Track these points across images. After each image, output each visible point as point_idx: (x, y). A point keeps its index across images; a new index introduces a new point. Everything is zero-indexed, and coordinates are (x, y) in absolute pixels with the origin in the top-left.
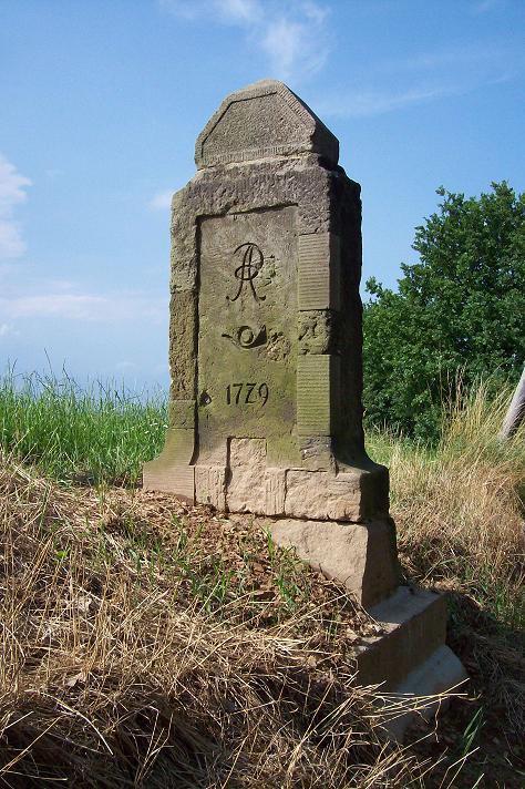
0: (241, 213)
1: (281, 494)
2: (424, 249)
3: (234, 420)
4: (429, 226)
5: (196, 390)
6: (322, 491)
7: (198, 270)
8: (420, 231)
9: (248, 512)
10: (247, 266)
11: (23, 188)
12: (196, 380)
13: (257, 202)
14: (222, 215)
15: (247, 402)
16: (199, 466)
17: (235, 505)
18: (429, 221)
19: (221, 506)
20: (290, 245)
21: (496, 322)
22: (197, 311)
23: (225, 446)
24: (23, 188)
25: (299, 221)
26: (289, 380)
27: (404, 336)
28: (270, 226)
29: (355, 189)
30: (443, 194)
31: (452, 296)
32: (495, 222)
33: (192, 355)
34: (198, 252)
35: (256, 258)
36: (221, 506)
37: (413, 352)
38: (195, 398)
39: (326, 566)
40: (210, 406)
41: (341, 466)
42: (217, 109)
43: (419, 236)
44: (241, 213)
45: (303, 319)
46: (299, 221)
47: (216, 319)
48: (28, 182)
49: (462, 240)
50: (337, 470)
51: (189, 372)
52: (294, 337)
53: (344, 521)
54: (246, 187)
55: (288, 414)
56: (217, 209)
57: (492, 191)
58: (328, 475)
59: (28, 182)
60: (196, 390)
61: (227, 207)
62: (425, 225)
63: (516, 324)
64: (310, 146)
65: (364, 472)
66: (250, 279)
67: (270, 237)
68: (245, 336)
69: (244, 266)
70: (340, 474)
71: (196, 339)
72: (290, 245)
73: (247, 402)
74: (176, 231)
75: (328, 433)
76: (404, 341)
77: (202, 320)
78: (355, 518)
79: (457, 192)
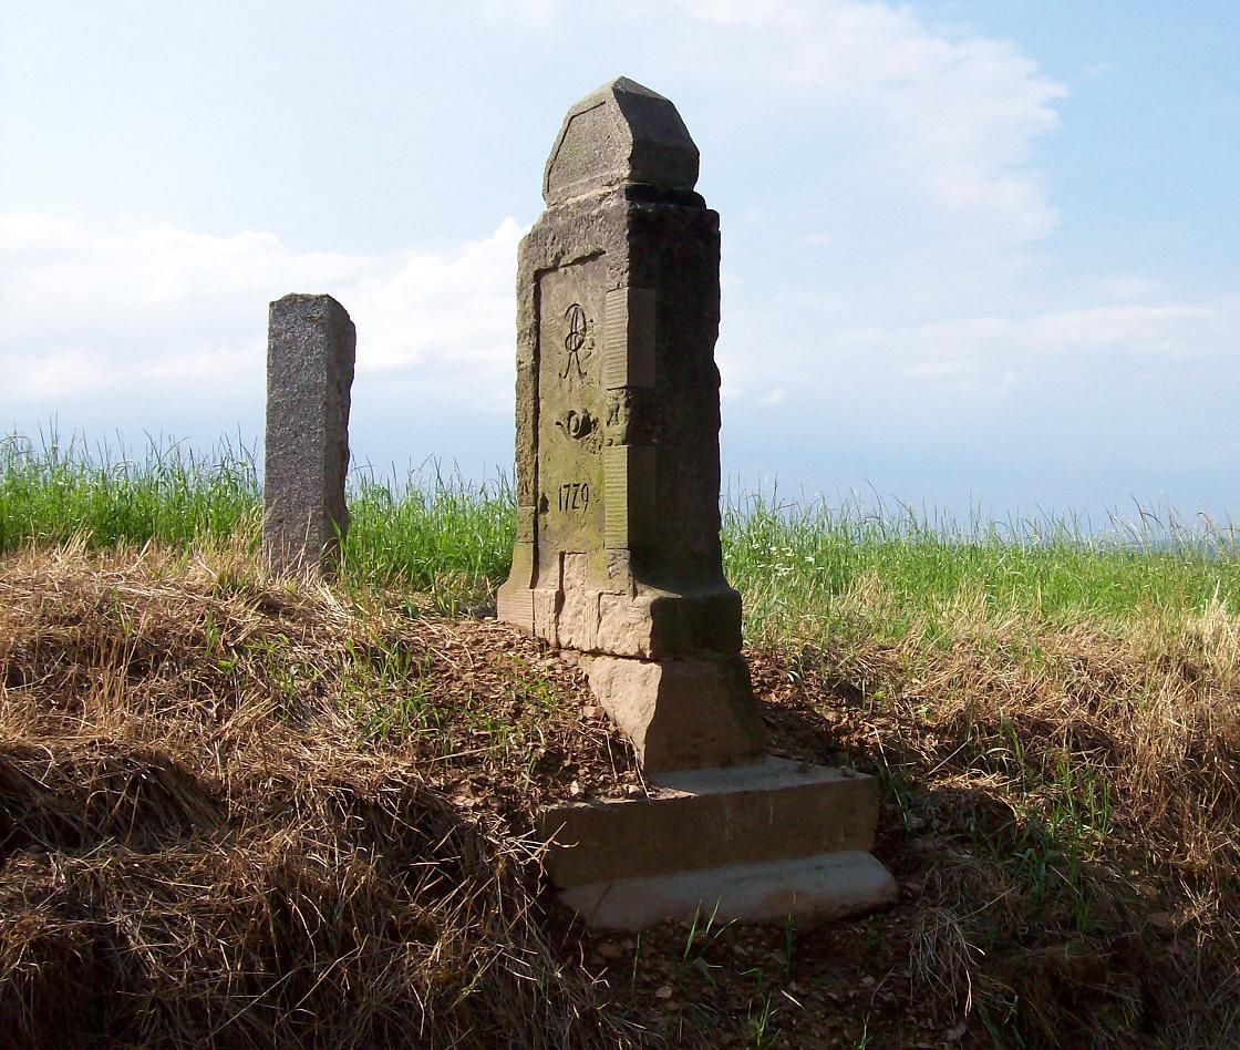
0: (568, 265)
1: (595, 624)
5: (536, 493)
7: (538, 340)
9: (573, 648)
11: (1053, 103)
12: (536, 480)
14: (554, 269)
15: (574, 508)
16: (536, 590)
17: (564, 641)
19: (552, 641)
22: (537, 392)
23: (557, 564)
24: (1053, 103)
29: (704, 227)
33: (532, 448)
34: (538, 316)
36: (552, 641)
38: (536, 504)
39: (619, 716)
40: (549, 515)
41: (640, 587)
42: (560, 126)
44: (568, 265)
48: (1061, 91)
50: (635, 593)
56: (550, 262)
59: (1061, 91)
60: (536, 493)
61: (558, 259)
64: (628, 172)
65: (661, 593)
66: (575, 350)
69: (572, 333)
70: (639, 598)
71: (536, 428)
73: (574, 508)
74: (521, 289)
75: (626, 546)
77: (542, 403)
78: (648, 653)
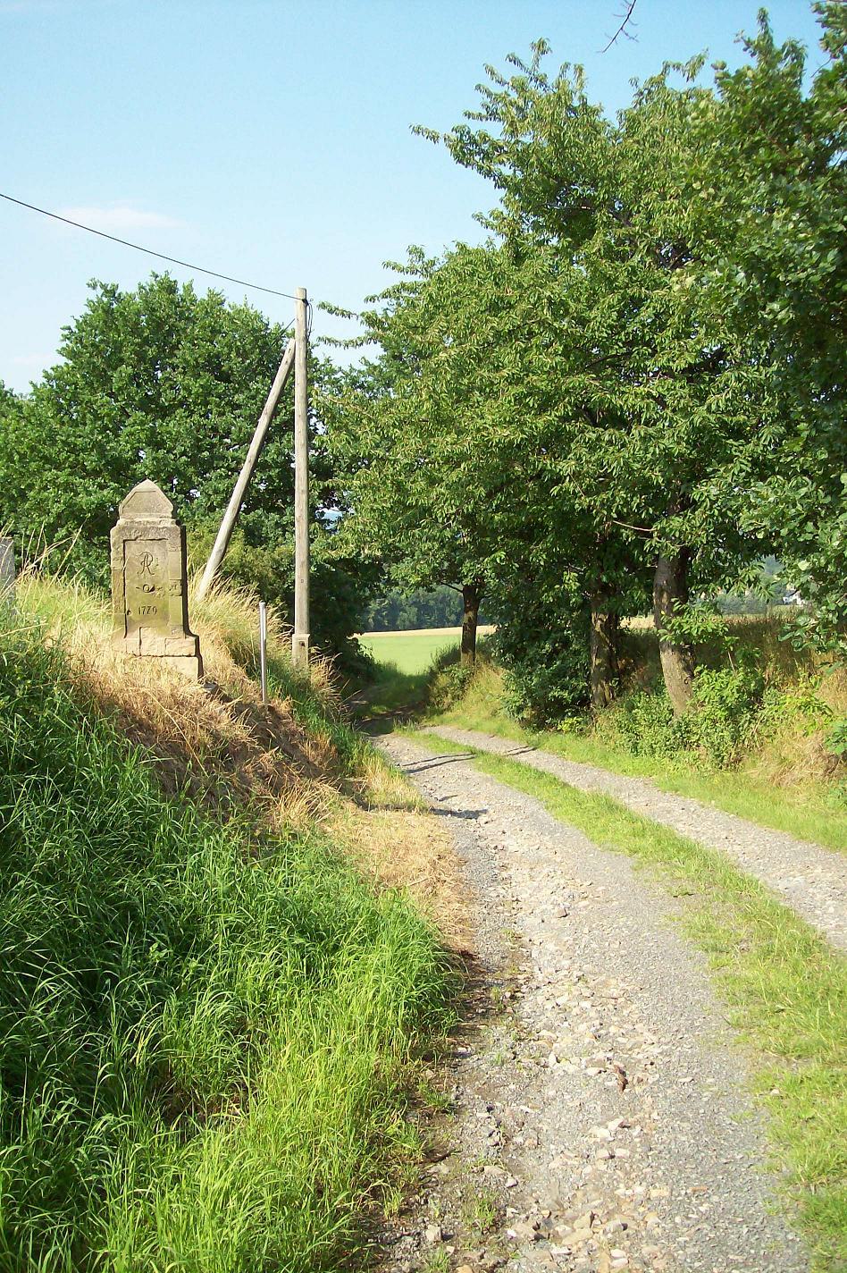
2: (72, 354)
3: (142, 621)
4: (79, 325)
6: (180, 645)
8: (67, 332)
10: (146, 561)
13: (151, 537)
18: (77, 321)
20: (165, 554)
21: (162, 452)
25: (168, 546)
26: (166, 605)
27: (47, 459)
28: (156, 548)
30: (94, 288)
31: (108, 415)
32: (158, 324)
35: (150, 558)
37: (60, 480)
43: (66, 338)
45: (171, 583)
46: (168, 546)
47: (132, 580)
49: (118, 347)
51: (122, 602)
52: (167, 589)
53: (189, 656)
54: (146, 530)
55: (165, 618)
57: (151, 280)
58: (183, 639)
62: (73, 325)
63: (183, 454)
67: (156, 550)
68: (146, 588)
72: (165, 554)
76: (47, 466)
79: (109, 281)
